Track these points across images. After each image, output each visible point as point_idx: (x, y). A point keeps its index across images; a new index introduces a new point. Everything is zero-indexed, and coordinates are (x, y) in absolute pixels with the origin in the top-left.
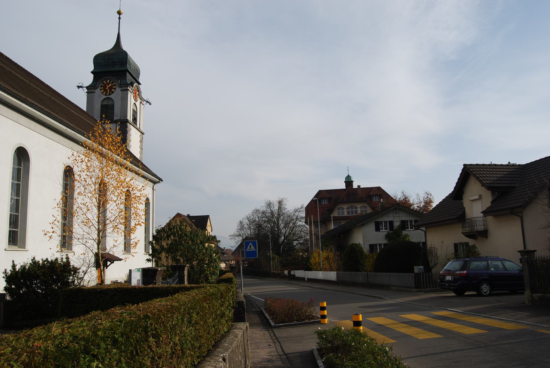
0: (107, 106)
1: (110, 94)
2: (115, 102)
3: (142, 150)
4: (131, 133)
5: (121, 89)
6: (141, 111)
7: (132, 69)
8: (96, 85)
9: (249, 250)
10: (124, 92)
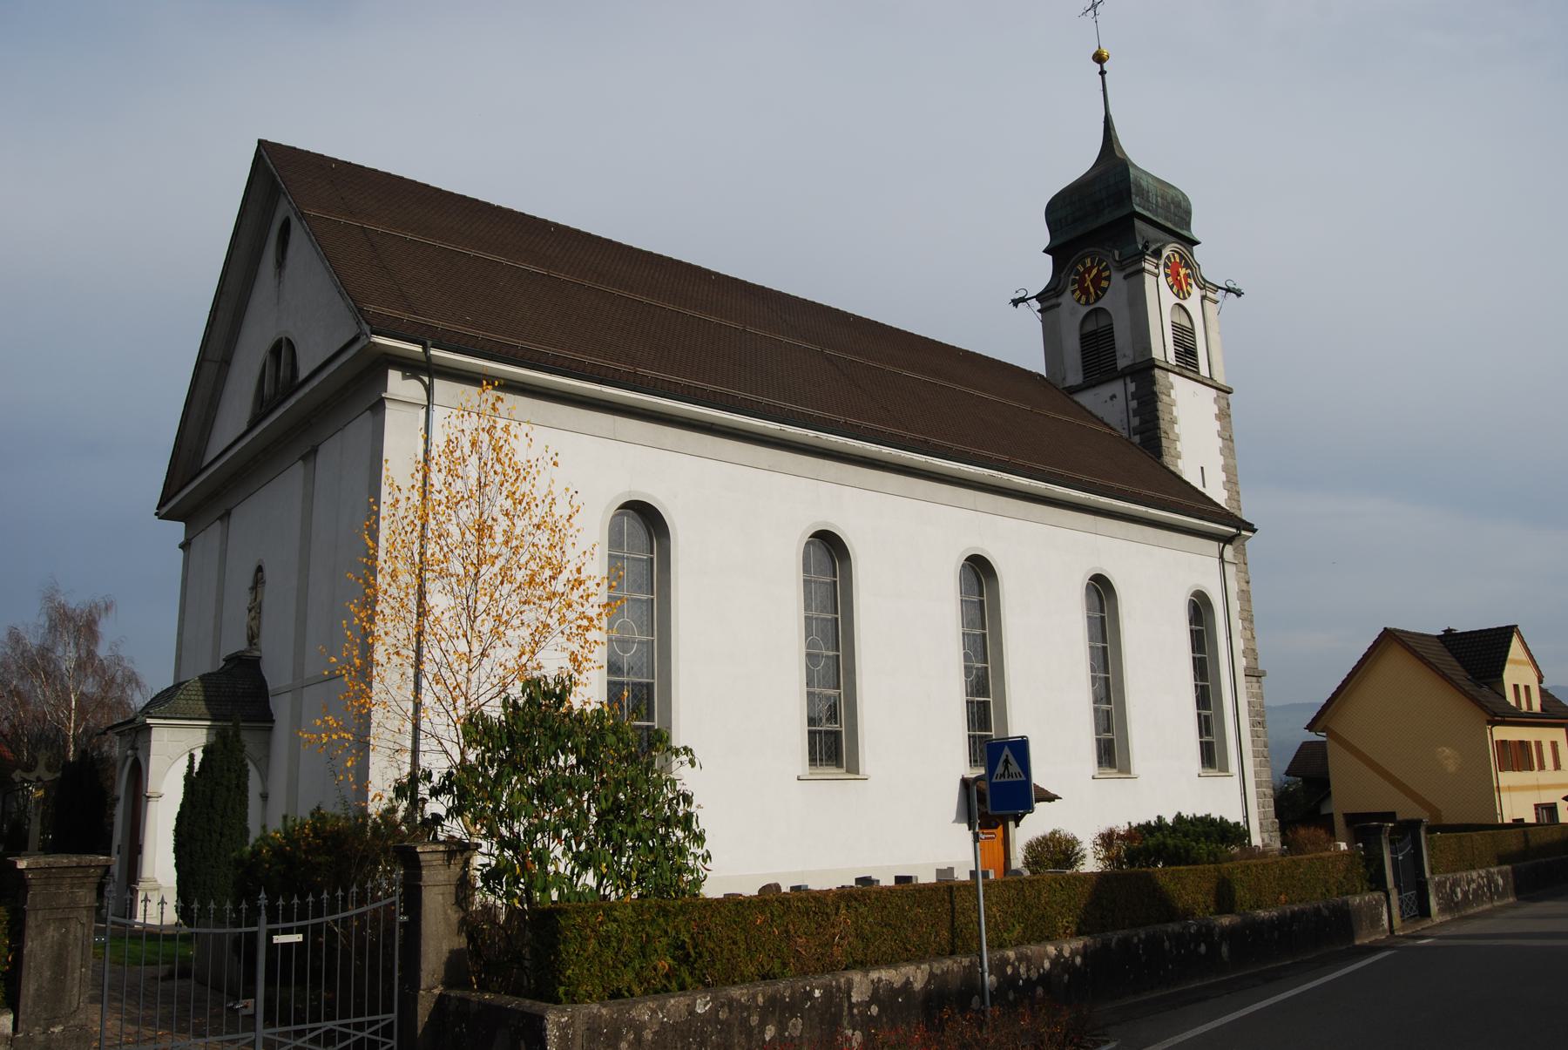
0: (1093, 335)
1: (1098, 298)
2: (1113, 317)
3: (1232, 441)
5: (1123, 274)
6: (1208, 324)
7: (1157, 206)
8: (1058, 285)
9: (1002, 780)
10: (1134, 279)
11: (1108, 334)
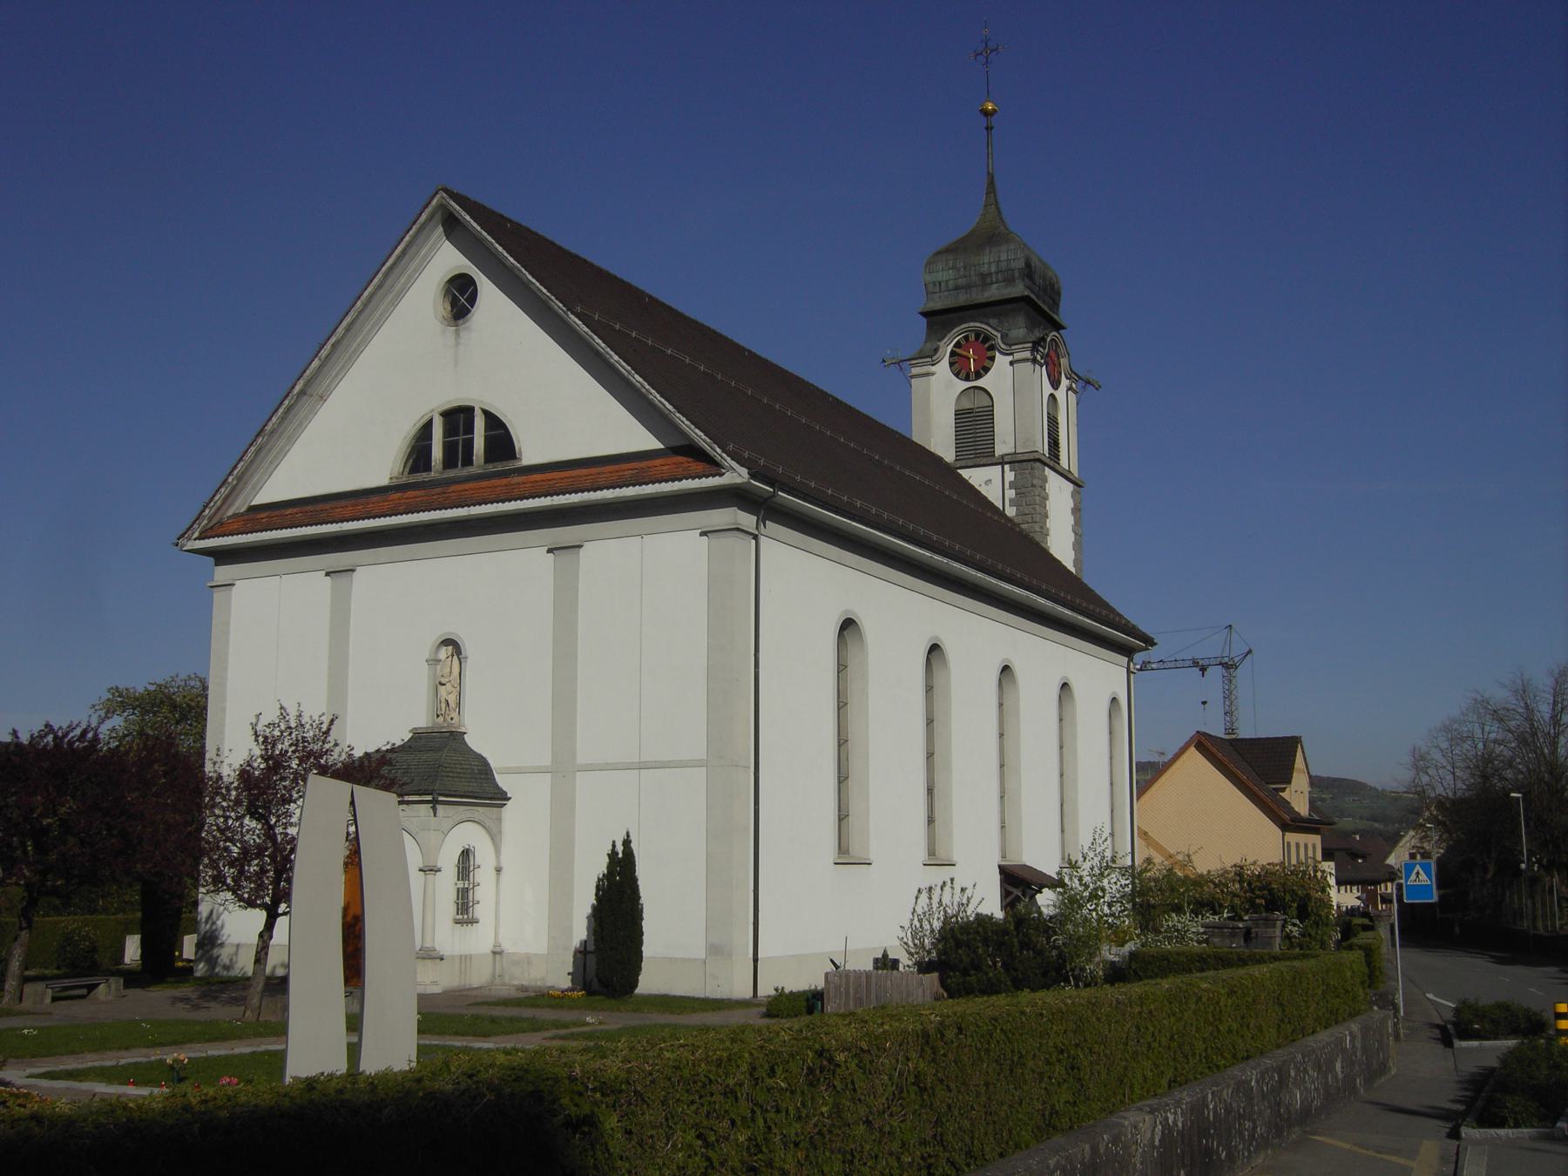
1: (978, 376)
4: (1047, 491)
5: (1010, 358)
11: (988, 414)
